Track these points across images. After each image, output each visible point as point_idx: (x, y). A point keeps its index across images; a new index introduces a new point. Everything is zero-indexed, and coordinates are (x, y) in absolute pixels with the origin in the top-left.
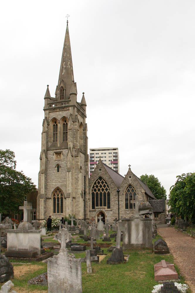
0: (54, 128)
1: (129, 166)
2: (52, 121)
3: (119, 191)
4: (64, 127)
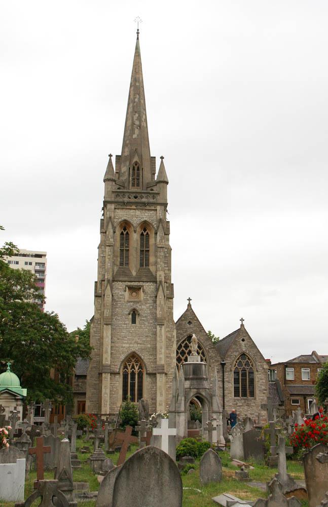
0: (122, 239)
1: (240, 320)
2: (120, 226)
3: (225, 364)
4: (142, 239)
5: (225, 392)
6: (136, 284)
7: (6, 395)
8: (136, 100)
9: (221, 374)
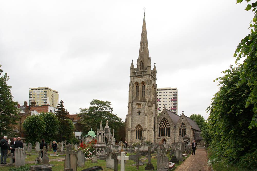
0: (136, 88)
3: (176, 127)
5: (176, 136)
6: (140, 103)
7: (89, 137)
8: (143, 38)
9: (174, 130)
